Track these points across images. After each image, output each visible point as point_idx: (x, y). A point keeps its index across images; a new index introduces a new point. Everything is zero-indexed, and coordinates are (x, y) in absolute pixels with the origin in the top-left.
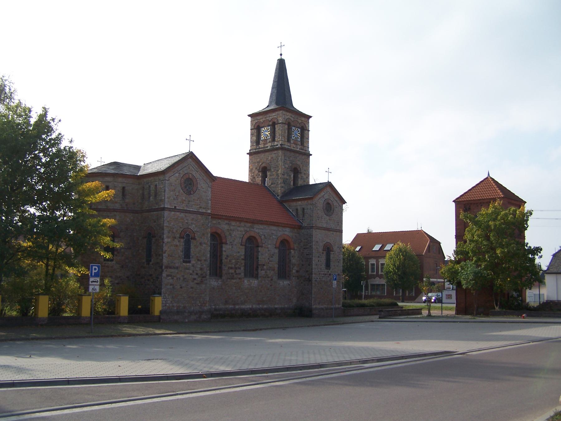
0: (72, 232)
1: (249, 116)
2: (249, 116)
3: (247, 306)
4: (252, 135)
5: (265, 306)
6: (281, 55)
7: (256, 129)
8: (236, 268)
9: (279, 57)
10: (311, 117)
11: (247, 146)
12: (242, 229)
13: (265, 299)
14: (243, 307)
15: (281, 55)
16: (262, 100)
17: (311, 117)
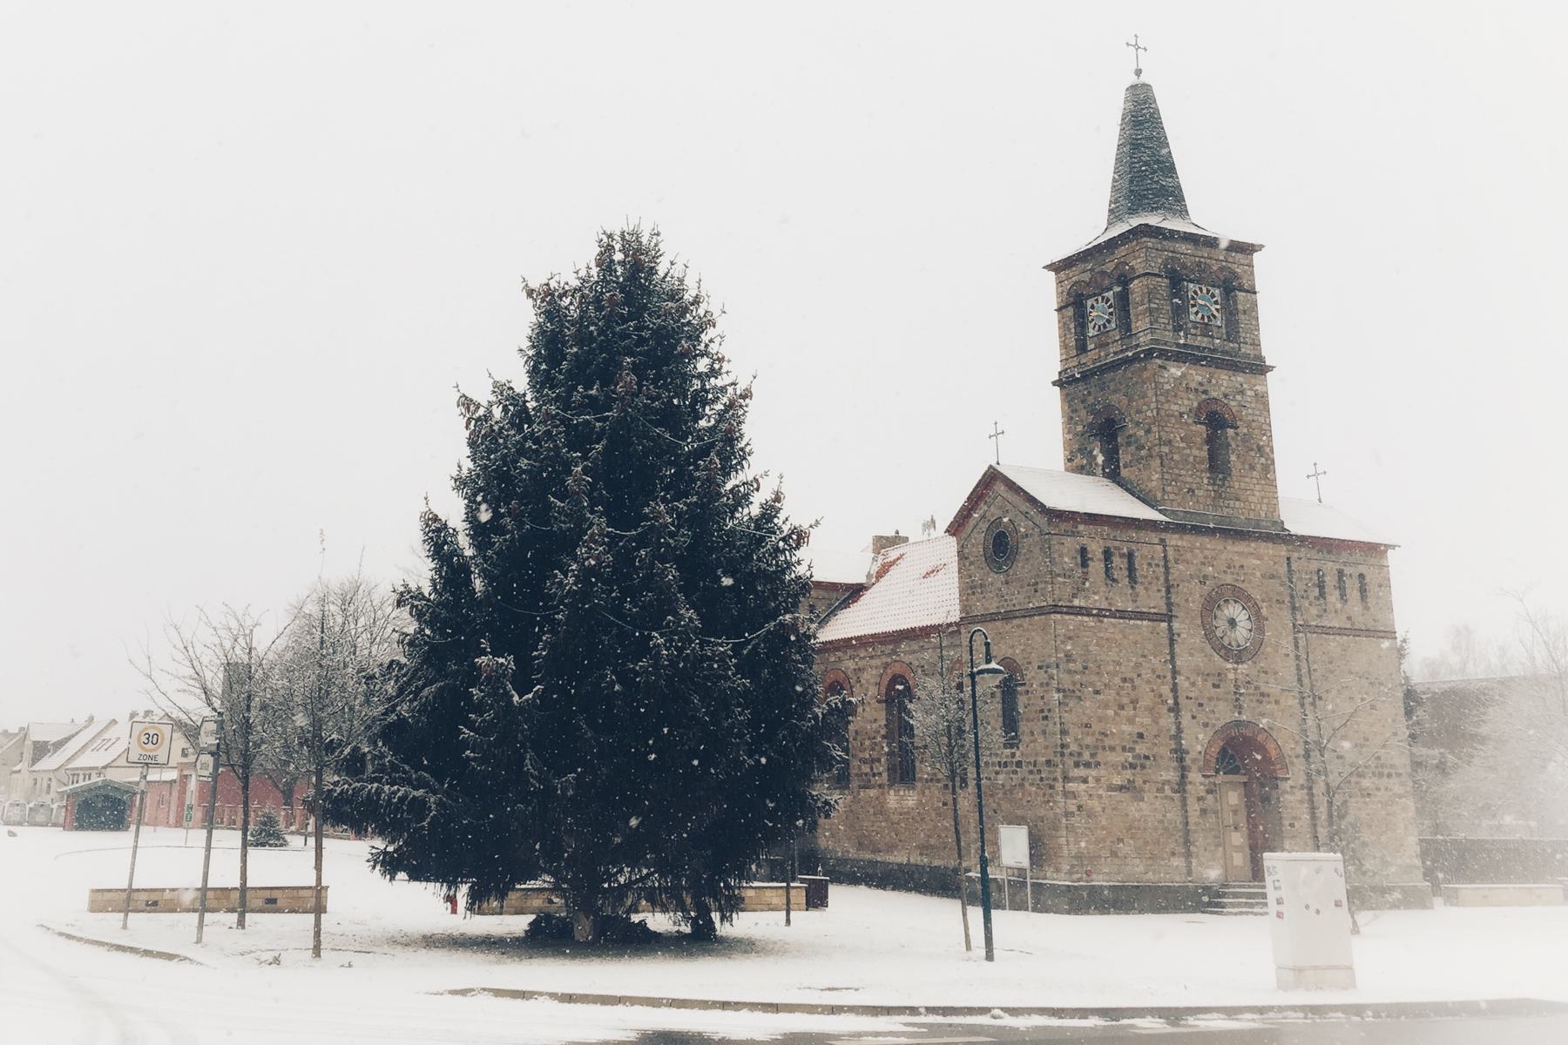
0: (763, 760)
1: (1050, 267)
2: (1050, 267)
3: (899, 858)
4: (1064, 327)
5: (936, 863)
6: (1138, 72)
7: (1074, 306)
8: (873, 761)
9: (1133, 80)
10: (1259, 248)
11: (1052, 364)
12: (877, 662)
13: (932, 841)
14: (890, 858)
15: (1138, 72)
16: (1087, 220)
17: (1259, 248)
